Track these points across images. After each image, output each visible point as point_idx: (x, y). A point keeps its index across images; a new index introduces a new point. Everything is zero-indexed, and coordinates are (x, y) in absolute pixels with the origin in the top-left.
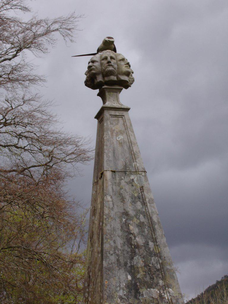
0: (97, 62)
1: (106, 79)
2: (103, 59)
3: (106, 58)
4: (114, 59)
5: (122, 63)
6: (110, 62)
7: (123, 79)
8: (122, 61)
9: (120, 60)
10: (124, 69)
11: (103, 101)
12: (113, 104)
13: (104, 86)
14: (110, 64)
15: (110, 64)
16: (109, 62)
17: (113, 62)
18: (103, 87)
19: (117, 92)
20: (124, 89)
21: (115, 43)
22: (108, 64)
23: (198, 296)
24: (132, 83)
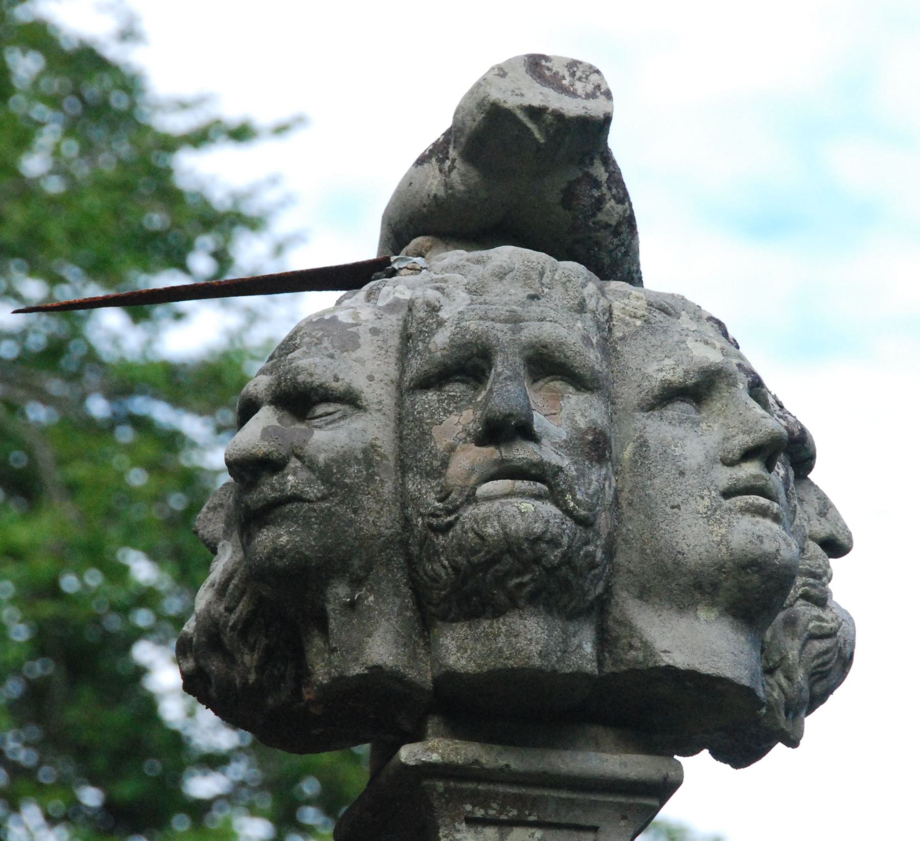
0: (351, 400)
1: (460, 650)
2: (437, 378)
3: (469, 365)
4: (581, 381)
5: (693, 443)
6: (525, 431)
7: (680, 660)
8: (680, 408)
9: (669, 395)
10: (705, 528)
11: (835, 688)
12: (522, 373)
13: (417, 736)
14: (523, 452)
15: (523, 452)
16: (502, 430)
17: (561, 418)
18: (408, 754)
19: (595, 829)
20: (700, 769)
21: (617, 141)
22: (490, 453)
23: (359, 337)
24: (816, 700)
